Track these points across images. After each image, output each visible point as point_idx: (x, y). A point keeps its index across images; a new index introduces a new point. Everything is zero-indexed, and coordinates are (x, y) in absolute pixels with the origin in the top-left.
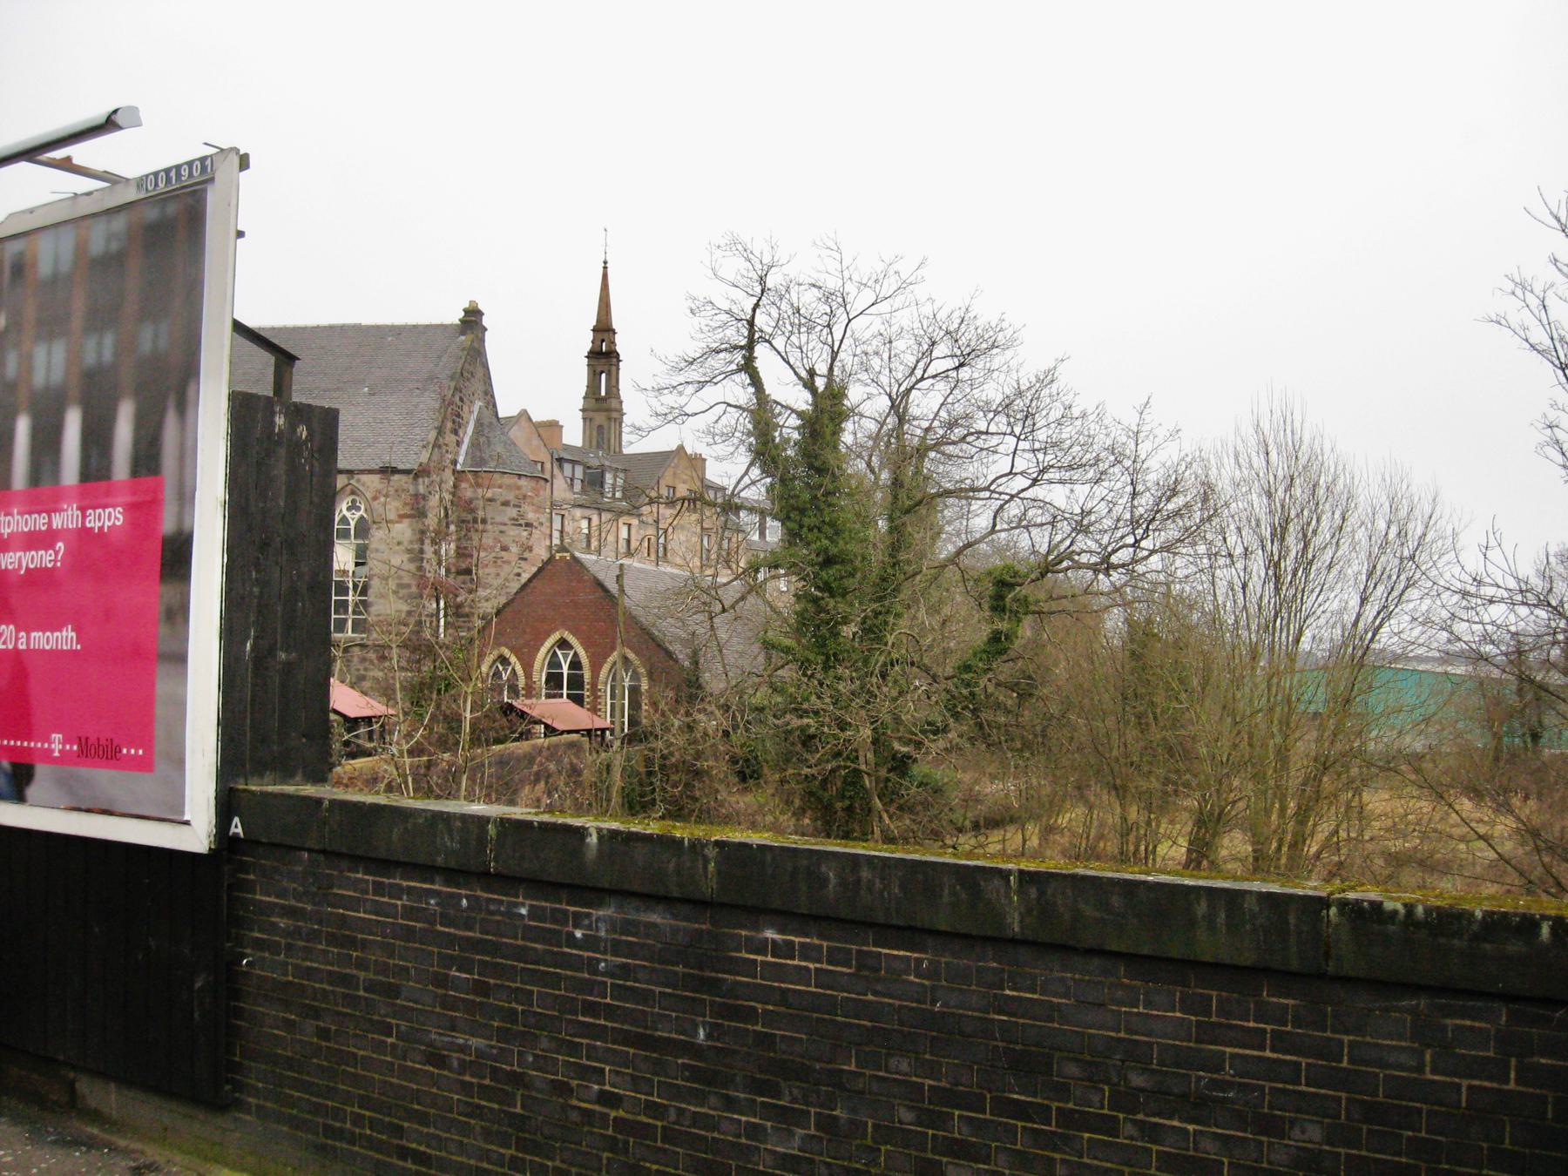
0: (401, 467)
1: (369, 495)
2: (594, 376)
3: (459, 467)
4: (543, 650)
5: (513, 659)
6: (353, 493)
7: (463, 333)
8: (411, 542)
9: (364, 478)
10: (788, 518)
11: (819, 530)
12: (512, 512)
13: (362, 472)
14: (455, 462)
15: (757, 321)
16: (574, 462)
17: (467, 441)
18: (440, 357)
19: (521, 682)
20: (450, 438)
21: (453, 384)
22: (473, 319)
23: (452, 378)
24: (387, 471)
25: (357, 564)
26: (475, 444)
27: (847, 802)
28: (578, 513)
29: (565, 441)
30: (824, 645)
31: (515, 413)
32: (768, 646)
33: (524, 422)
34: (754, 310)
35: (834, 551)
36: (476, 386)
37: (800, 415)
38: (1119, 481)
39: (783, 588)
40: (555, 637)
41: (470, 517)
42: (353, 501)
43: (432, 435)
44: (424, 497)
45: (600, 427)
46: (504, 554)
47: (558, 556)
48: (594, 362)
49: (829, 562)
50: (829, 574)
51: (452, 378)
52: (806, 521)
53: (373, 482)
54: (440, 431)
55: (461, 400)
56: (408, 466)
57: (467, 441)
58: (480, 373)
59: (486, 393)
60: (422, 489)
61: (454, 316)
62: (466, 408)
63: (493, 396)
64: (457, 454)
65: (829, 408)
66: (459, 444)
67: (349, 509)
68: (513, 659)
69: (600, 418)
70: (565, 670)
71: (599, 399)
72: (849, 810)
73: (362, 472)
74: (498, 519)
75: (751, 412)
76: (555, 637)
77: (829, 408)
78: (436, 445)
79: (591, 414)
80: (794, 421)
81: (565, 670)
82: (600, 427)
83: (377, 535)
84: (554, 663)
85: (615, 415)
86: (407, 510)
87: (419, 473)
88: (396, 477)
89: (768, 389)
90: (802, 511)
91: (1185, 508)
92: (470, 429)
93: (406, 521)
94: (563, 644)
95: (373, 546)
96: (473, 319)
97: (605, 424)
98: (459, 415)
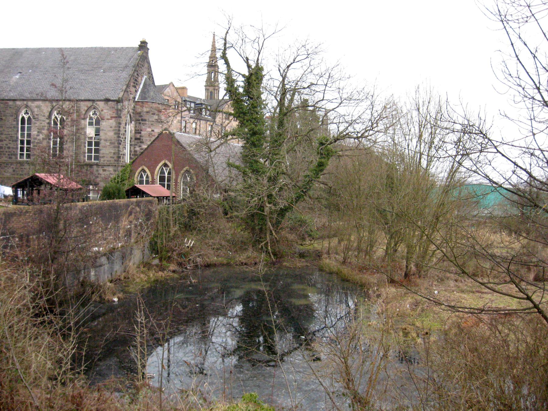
0: (112, 99)
1: (100, 109)
2: (209, 73)
3: (136, 100)
4: (158, 167)
5: (147, 170)
6: (94, 108)
7: (139, 50)
8: (115, 127)
9: (98, 103)
10: (239, 116)
11: (251, 121)
12: (156, 117)
13: (98, 100)
14: (135, 98)
15: (227, 39)
16: (191, 102)
17: (140, 90)
18: (130, 59)
19: (150, 179)
20: (133, 89)
21: (134, 69)
22: (143, 46)
23: (134, 67)
24: (107, 100)
25: (96, 135)
26: (143, 92)
27: (260, 226)
28: (192, 120)
29: (188, 94)
30: (252, 166)
31: (168, 83)
32: (229, 165)
33: (171, 87)
34: (226, 34)
35: (256, 129)
36: (145, 70)
37: (244, 76)
38: (366, 104)
39: (237, 144)
40: (163, 162)
41: (140, 118)
42: (95, 111)
43: (125, 87)
44: (120, 110)
45: (211, 92)
46: (152, 132)
47: (164, 132)
48: (210, 69)
49: (254, 134)
50: (254, 139)
51: (134, 67)
52: (246, 118)
53: (101, 104)
54: (128, 86)
55: (137, 75)
56: (115, 99)
57: (140, 90)
58: (146, 65)
59: (149, 73)
60: (119, 107)
61: (136, 44)
62: (140, 78)
63: (152, 74)
64: (136, 95)
65: (255, 76)
66: (136, 91)
67: (93, 114)
68: (147, 170)
69: (211, 89)
70: (166, 175)
71: (211, 83)
72: (261, 229)
73: (98, 100)
74: (151, 120)
75: (218, 72)
76: (163, 162)
77: (255, 76)
78: (126, 91)
79: (208, 87)
80: (241, 79)
81: (166, 175)
82: (211, 92)
83: (104, 124)
84: (162, 172)
85: (217, 88)
86: (114, 115)
87: (118, 101)
88: (110, 103)
89: (232, 66)
90: (244, 114)
91: (390, 115)
92: (141, 86)
93: (114, 119)
94: (165, 165)
95: (101, 128)
96: (143, 46)
97: (213, 91)
98: (136, 80)
